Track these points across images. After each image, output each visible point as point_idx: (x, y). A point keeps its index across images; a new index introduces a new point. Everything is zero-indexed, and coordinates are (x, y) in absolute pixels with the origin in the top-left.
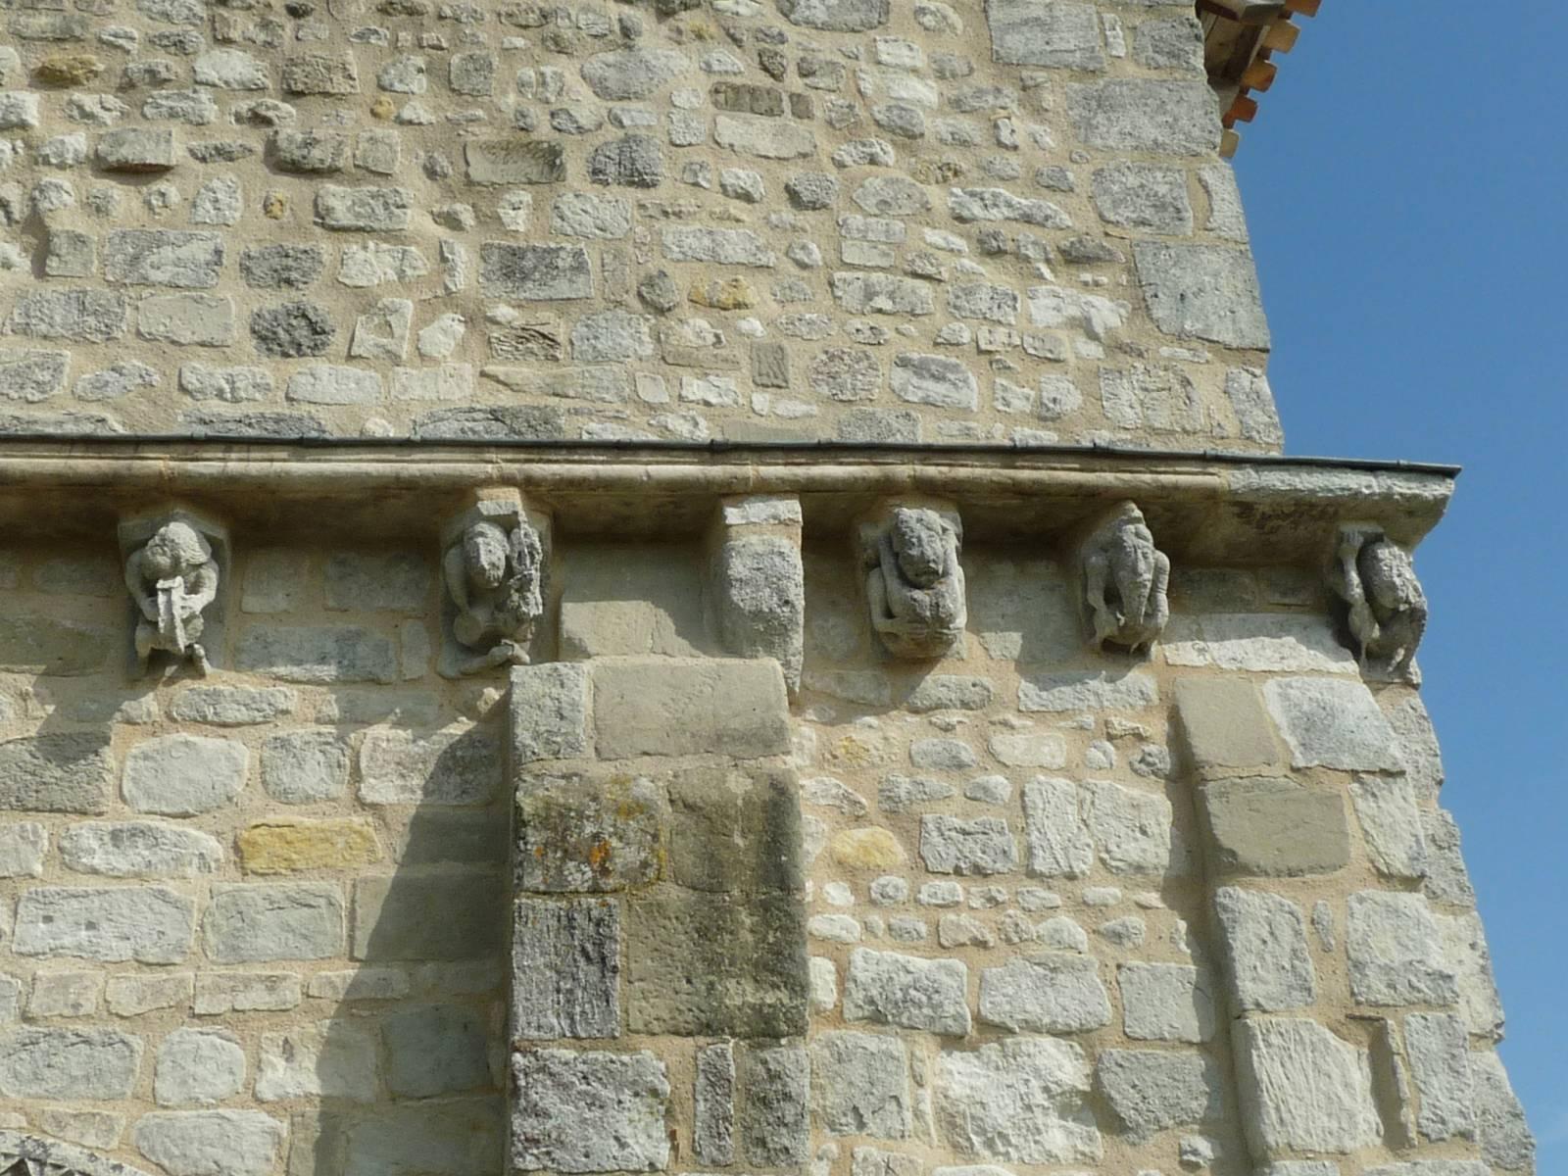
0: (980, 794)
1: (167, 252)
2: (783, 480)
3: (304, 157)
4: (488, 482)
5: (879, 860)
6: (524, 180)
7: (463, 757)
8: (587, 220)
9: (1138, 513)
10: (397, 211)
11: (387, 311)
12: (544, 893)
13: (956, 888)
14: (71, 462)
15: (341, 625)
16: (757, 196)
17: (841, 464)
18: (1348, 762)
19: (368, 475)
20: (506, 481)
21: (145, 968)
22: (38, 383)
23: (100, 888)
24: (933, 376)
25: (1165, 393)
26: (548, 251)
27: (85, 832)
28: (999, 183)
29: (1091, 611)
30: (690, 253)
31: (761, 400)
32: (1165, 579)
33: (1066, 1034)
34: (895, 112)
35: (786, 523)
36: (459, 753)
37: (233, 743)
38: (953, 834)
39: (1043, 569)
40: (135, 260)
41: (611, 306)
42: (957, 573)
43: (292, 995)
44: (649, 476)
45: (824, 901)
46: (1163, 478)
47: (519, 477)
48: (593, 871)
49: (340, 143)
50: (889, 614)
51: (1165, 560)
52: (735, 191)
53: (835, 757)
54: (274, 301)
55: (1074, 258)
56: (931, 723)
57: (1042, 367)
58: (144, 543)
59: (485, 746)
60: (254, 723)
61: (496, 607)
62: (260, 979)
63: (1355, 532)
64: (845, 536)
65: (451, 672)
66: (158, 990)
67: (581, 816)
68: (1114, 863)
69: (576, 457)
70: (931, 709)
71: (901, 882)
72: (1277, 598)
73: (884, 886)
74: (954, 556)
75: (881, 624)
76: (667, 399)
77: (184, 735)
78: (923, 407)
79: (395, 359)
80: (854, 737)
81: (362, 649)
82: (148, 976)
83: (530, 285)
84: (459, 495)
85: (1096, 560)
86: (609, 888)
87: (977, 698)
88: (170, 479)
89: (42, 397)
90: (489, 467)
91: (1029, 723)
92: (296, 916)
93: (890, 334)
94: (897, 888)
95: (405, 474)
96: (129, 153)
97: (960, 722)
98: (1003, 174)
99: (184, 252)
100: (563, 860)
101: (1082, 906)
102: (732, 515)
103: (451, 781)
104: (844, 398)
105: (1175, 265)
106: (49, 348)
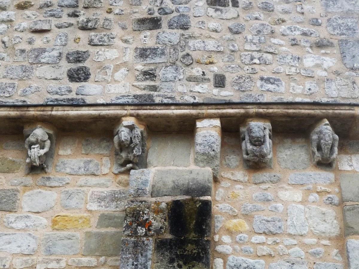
0: (273, 209)
1: (46, 54)
2: (215, 114)
3: (86, 25)
4: (126, 116)
5: (240, 229)
6: (148, 29)
7: (117, 197)
8: (165, 39)
9: (327, 122)
10: (112, 40)
12: (131, 236)
13: (262, 238)
14: (10, 112)
15: (86, 159)
16: (219, 31)
17: (233, 109)
19: (91, 114)
20: (131, 115)
21: (24, 256)
22: (8, 92)
23: (13, 233)
24: (271, 83)
25: (347, 86)
26: (155, 49)
27: (11, 217)
28: (297, 24)
30: (197, 48)
31: (216, 91)
32: (337, 144)
34: (264, 4)
35: (215, 127)
36: (116, 196)
37: (53, 192)
38: (264, 221)
40: (37, 57)
41: (172, 64)
42: (268, 141)
44: (173, 113)
45: (222, 241)
46: (336, 111)
47: (135, 115)
48: (146, 229)
49: (97, 21)
51: (337, 137)
52: (213, 30)
53: (229, 197)
54: (74, 66)
55: (320, 45)
56: (260, 188)
57: (307, 79)
58: (29, 135)
59: (124, 194)
60: (59, 187)
61: (128, 152)
62: (55, 260)
65: (116, 172)
66: (26, 262)
67: (143, 213)
68: (315, 231)
69: (152, 108)
70: (260, 183)
71: (246, 236)
73: (241, 237)
74: (268, 137)
75: (245, 156)
76: (185, 91)
77: (40, 190)
78: (267, 92)
80: (235, 192)
81: (91, 165)
82: (25, 258)
83: (148, 59)
84: (116, 120)
85: (315, 137)
86: (150, 235)
87: (275, 180)
88: (36, 117)
89: (9, 95)
90: (126, 112)
91: (291, 188)
92: (66, 242)
94: (244, 237)
95: (101, 114)
96: (38, 27)
97: (269, 187)
98: (298, 21)
99: (51, 54)
100: (137, 226)
101: (303, 245)
102: (199, 124)
103: (114, 204)
104: (242, 90)
105: (352, 47)
106: (12, 81)
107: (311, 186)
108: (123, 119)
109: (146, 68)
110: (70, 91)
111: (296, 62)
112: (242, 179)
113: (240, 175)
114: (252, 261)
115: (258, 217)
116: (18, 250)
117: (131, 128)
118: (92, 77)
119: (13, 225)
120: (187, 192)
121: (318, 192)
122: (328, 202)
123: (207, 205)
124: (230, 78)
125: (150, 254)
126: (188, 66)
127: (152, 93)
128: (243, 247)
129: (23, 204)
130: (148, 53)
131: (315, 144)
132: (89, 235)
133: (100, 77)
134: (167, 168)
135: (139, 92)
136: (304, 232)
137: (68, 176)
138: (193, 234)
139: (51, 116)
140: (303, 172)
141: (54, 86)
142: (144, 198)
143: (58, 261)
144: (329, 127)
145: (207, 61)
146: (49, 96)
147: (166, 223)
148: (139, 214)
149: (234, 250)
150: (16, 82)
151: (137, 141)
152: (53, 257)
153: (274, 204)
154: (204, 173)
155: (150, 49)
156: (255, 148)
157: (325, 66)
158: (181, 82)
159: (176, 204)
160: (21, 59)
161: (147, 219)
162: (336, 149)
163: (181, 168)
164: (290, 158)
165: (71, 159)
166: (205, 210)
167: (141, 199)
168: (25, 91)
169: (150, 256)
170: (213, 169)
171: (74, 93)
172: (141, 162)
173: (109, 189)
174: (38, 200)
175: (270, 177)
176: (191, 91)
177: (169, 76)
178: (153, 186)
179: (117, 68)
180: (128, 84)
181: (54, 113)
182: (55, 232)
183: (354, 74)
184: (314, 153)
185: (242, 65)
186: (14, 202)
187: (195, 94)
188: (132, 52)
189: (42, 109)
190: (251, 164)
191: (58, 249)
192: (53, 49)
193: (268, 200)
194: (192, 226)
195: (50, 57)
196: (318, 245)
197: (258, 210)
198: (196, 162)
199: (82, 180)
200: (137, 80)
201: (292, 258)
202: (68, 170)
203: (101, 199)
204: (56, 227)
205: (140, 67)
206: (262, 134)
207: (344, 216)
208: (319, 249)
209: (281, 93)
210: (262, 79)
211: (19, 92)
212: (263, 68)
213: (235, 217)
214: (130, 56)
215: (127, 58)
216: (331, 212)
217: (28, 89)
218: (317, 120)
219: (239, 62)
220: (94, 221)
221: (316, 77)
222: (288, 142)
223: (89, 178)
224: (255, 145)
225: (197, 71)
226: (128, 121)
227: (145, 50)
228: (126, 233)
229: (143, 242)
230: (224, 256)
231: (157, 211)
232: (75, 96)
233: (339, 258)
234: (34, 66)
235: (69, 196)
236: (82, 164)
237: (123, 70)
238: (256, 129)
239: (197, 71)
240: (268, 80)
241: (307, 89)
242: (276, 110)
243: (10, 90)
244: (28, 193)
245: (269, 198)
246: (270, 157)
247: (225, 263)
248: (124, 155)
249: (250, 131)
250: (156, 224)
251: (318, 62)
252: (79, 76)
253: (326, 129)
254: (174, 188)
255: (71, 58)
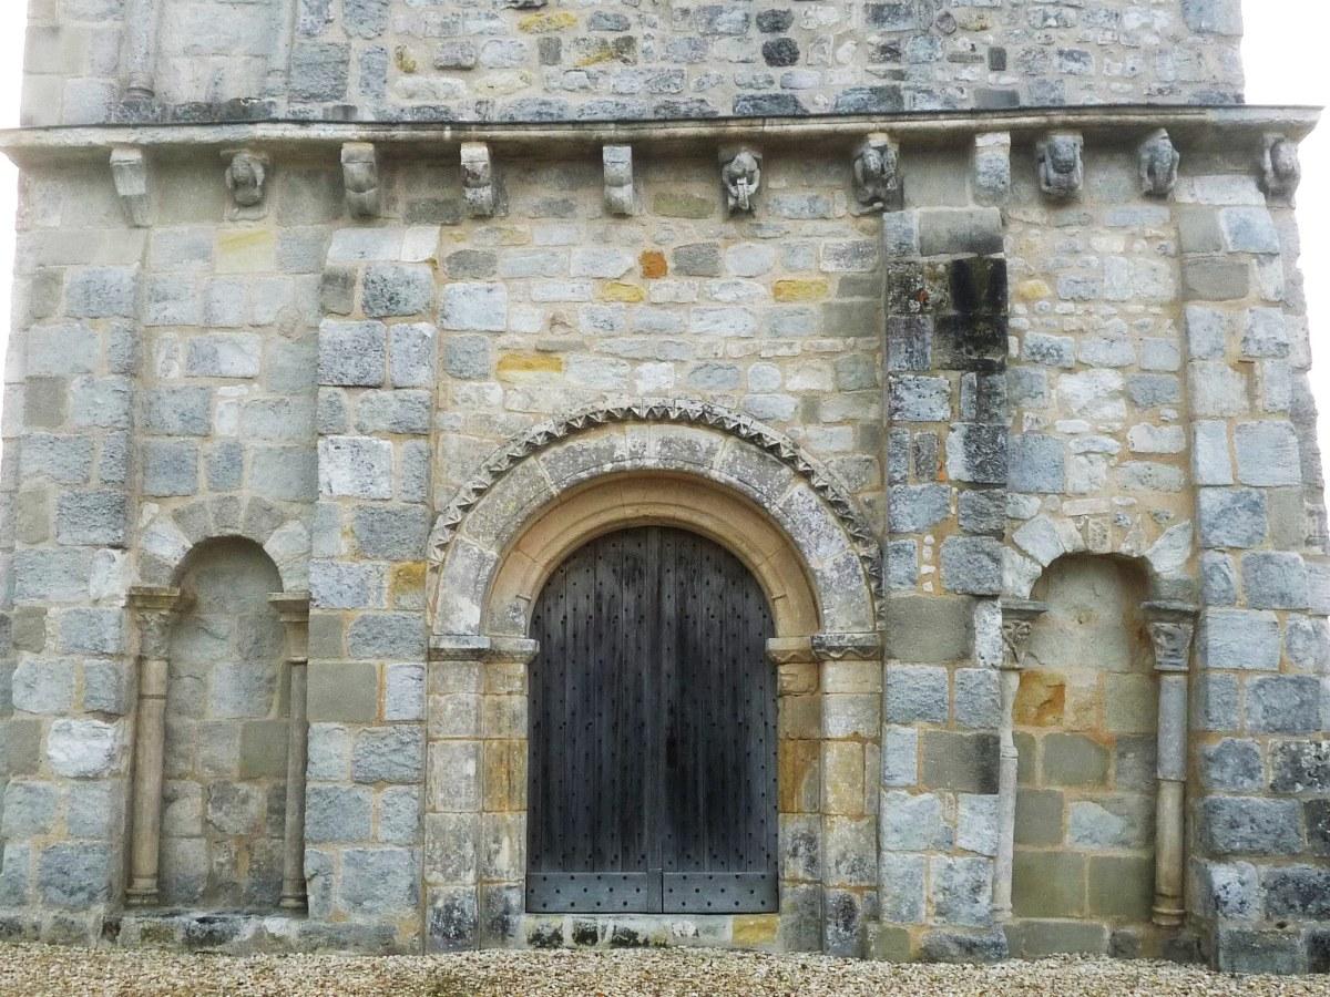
5: (1039, 294)
11: (822, 41)
13: (1070, 306)
15: (810, 193)
18: (1253, 249)
26: (895, 6)
27: (714, 284)
29: (1141, 179)
31: (992, 77)
33: (1116, 368)
35: (1003, 145)
39: (1121, 157)
40: (710, 22)
43: (798, 350)
46: (1180, 117)
50: (1048, 184)
51: (1177, 155)
54: (770, 38)
63: (1270, 137)
64: (1025, 147)
65: (857, 213)
70: (1064, 226)
72: (1232, 167)
75: (1045, 187)
77: (748, 243)
79: (825, 64)
82: (745, 342)
84: (860, 137)
85: (1146, 156)
92: (797, 318)
93: (1054, 39)
102: (980, 141)
106: (677, 66)
107: (1136, 229)
108: (870, 136)
109: (884, 41)
110: (772, 82)
111: (1113, 22)
112: (1038, 221)
113: (1036, 213)
114: (1057, 338)
115: (1065, 276)
116: (732, 332)
117: (882, 150)
118: (802, 56)
119: (719, 296)
120: (971, 247)
121: (1146, 238)
122: (1160, 252)
123: (1000, 266)
124: (1013, 52)
125: (928, 336)
126: (948, 34)
127: (897, 83)
128: (1044, 320)
129: (729, 266)
130: (885, 14)
131: (1145, 167)
132: (828, 307)
133: (815, 56)
134: (936, 209)
135: (878, 83)
136: (1127, 297)
137: (787, 222)
138: (984, 309)
139: (763, 133)
140: (1125, 208)
141: (744, 73)
142: (912, 258)
143: (790, 345)
144: (1168, 142)
145: (976, 25)
146: (740, 91)
147: (948, 294)
148: (909, 282)
149: (1032, 323)
150: (685, 68)
151: (891, 170)
152: (782, 340)
153: (1085, 257)
154: (988, 215)
155: (888, 5)
156: (1061, 177)
157: (1157, 27)
158: (940, 64)
159: (958, 264)
160: (684, 25)
161: (921, 290)
162: (1175, 172)
163: (956, 209)
164: (1104, 184)
165: (790, 195)
166: (999, 273)
167: (908, 259)
168: (700, 84)
169: (929, 340)
170: (1002, 210)
171: (777, 85)
172: (898, 201)
173: (850, 240)
174: (748, 259)
175: (1079, 216)
176: (956, 79)
177: (921, 53)
178: (921, 239)
179: (840, 39)
180: (859, 69)
181: (767, 129)
182: (781, 305)
183: (1201, 39)
184: (1141, 179)
185: (1031, 30)
186: (715, 263)
187: (963, 84)
188: (860, 11)
189: (749, 122)
190: (1053, 198)
191: (787, 328)
192: (734, 9)
193: (1076, 252)
194: (983, 297)
195: (730, 22)
196: (1145, 313)
197: (1062, 267)
198: (976, 199)
199: (808, 227)
200: (872, 61)
201: (1111, 333)
202: (786, 212)
203: (839, 255)
204: (781, 297)
205: (874, 38)
206: (1071, 155)
207: (1183, 274)
208: (1147, 320)
209: (1091, 76)
210: (1061, 53)
211: (692, 85)
212: (1063, 34)
213: (1031, 277)
214: (858, 20)
215: (854, 23)
216: (1164, 267)
217: (705, 79)
218: (1150, 129)
219: (1026, 23)
220: (833, 287)
221: (1143, 47)
222: (1103, 159)
223: (817, 223)
224: (1061, 172)
225: (962, 43)
226: (879, 140)
227: (880, 8)
228: (894, 309)
229: (918, 321)
230: (1020, 333)
231: (935, 278)
232: (779, 91)
233: (1174, 332)
234: (709, 39)
235: (793, 251)
236: (805, 203)
237: (849, 44)
238: (1063, 149)
239: (962, 43)
240: (1070, 55)
241: (1128, 68)
242: (1092, 118)
243: (678, 81)
244: (732, 248)
245: (1078, 248)
246: (1080, 188)
247: (1020, 342)
248: (870, 189)
249: (1054, 151)
250: (934, 296)
251: (1145, 20)
252: (780, 54)
253: (1163, 143)
254: (951, 242)
255: (765, 24)
